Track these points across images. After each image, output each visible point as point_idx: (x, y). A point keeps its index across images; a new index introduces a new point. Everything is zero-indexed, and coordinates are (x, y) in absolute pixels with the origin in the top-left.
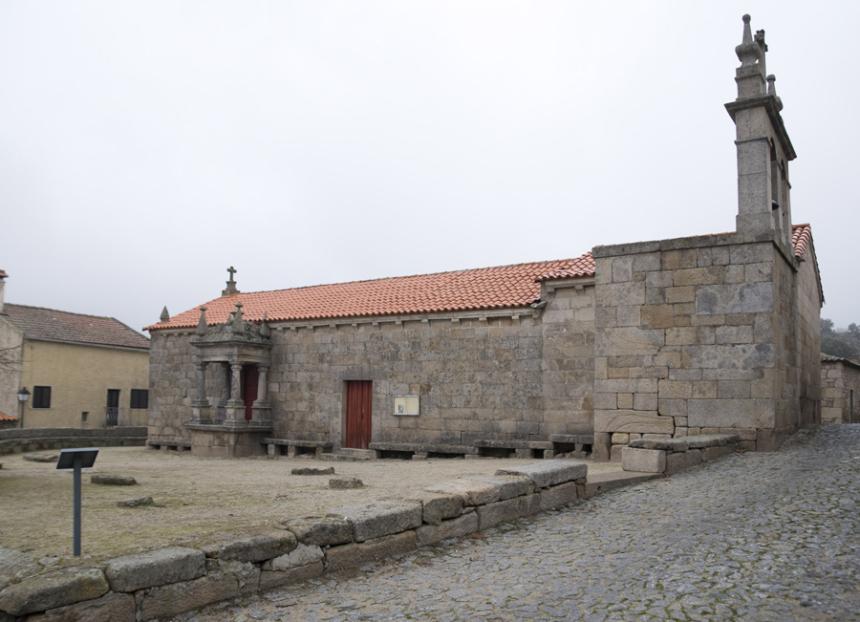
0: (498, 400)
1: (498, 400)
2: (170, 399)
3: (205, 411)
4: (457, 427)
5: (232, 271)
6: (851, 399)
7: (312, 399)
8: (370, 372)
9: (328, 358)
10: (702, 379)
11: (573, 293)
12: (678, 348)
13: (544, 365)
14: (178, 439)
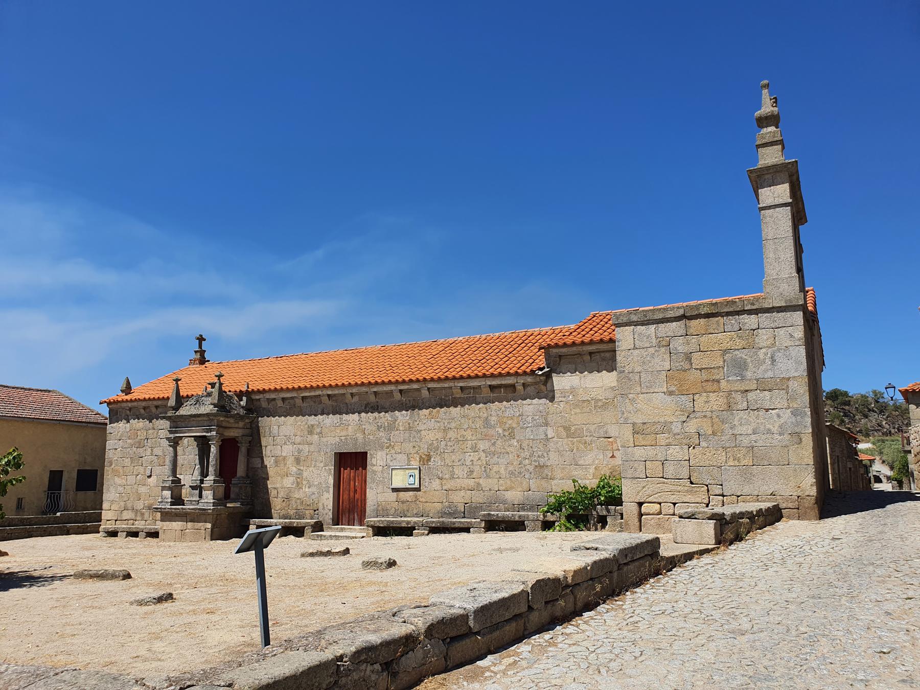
0: (502, 471)
1: (502, 471)
2: (131, 479)
4: (459, 499)
5: (201, 339)
6: (838, 465)
7: (299, 475)
9: (318, 430)
10: (736, 446)
12: (709, 414)
13: (550, 433)
14: (139, 525)
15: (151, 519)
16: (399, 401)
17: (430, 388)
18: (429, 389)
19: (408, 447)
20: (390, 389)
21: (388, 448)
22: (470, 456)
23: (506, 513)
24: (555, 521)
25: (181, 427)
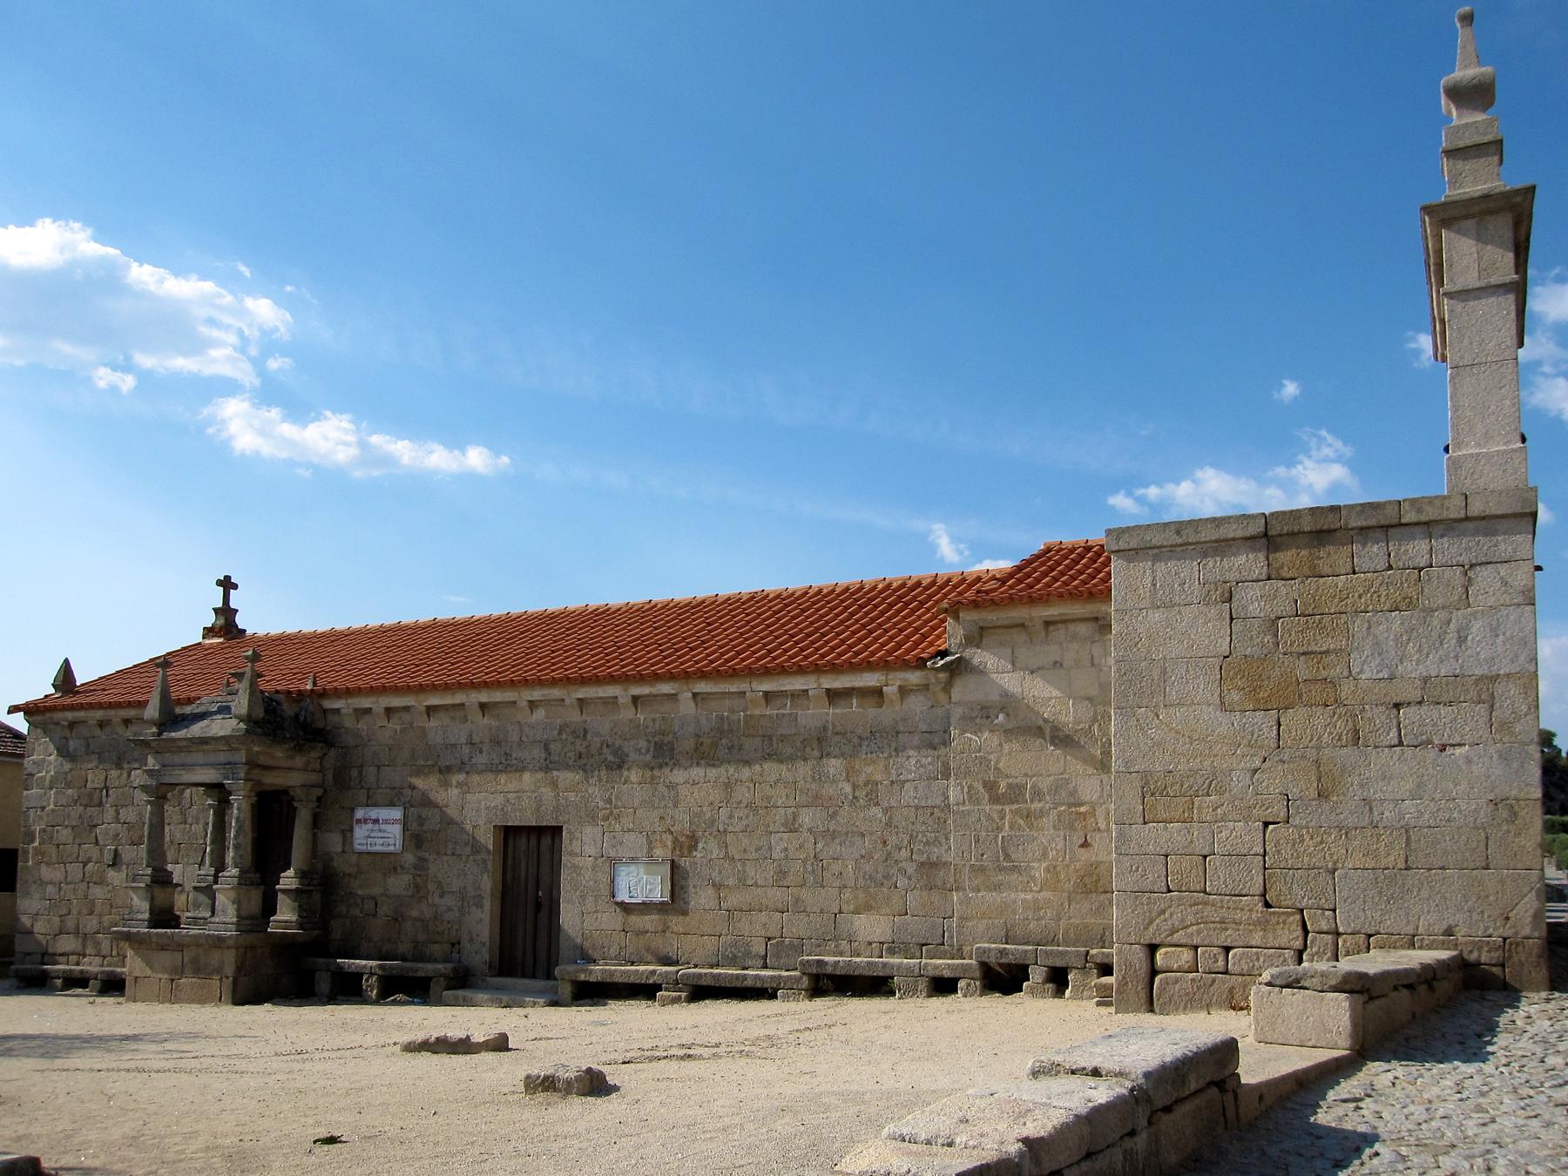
3: (160, 894)
8: (557, 809)
11: (1019, 637)
15: (114, 953)
16: (631, 721)
17: (698, 693)
18: (695, 695)
20: (611, 695)
21: (606, 818)
22: (781, 839)
23: (854, 959)
24: (959, 979)
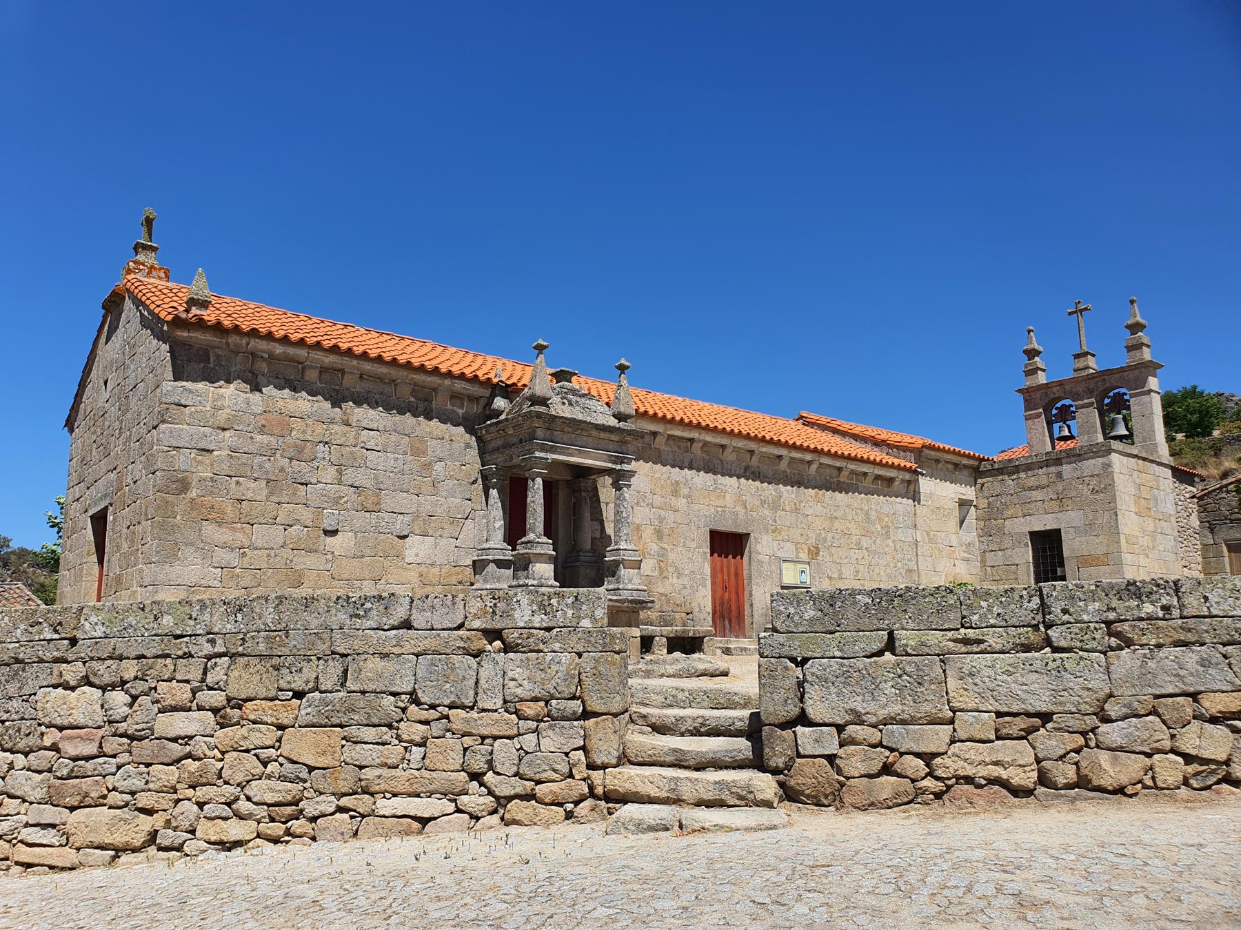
7: (662, 556)
9: (686, 491)
19: (795, 533)
21: (774, 532)
25: (561, 441)
